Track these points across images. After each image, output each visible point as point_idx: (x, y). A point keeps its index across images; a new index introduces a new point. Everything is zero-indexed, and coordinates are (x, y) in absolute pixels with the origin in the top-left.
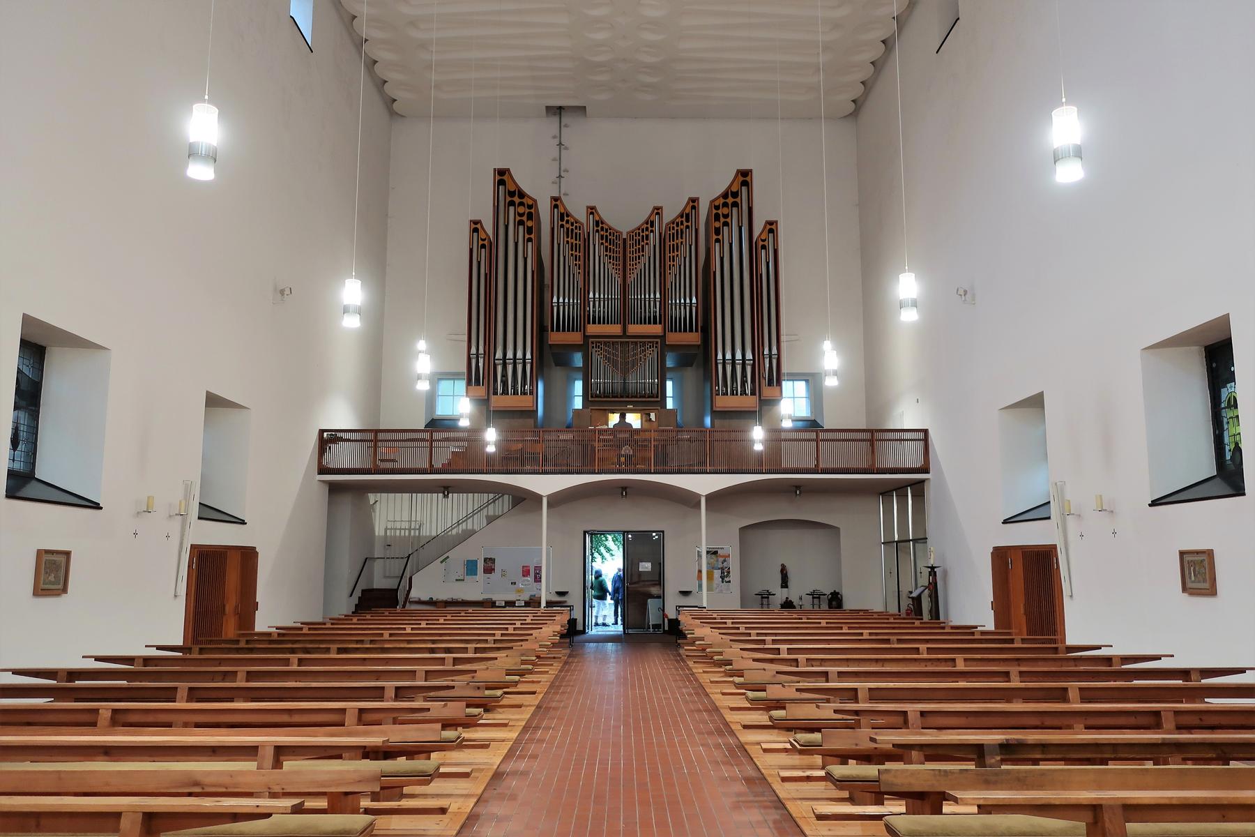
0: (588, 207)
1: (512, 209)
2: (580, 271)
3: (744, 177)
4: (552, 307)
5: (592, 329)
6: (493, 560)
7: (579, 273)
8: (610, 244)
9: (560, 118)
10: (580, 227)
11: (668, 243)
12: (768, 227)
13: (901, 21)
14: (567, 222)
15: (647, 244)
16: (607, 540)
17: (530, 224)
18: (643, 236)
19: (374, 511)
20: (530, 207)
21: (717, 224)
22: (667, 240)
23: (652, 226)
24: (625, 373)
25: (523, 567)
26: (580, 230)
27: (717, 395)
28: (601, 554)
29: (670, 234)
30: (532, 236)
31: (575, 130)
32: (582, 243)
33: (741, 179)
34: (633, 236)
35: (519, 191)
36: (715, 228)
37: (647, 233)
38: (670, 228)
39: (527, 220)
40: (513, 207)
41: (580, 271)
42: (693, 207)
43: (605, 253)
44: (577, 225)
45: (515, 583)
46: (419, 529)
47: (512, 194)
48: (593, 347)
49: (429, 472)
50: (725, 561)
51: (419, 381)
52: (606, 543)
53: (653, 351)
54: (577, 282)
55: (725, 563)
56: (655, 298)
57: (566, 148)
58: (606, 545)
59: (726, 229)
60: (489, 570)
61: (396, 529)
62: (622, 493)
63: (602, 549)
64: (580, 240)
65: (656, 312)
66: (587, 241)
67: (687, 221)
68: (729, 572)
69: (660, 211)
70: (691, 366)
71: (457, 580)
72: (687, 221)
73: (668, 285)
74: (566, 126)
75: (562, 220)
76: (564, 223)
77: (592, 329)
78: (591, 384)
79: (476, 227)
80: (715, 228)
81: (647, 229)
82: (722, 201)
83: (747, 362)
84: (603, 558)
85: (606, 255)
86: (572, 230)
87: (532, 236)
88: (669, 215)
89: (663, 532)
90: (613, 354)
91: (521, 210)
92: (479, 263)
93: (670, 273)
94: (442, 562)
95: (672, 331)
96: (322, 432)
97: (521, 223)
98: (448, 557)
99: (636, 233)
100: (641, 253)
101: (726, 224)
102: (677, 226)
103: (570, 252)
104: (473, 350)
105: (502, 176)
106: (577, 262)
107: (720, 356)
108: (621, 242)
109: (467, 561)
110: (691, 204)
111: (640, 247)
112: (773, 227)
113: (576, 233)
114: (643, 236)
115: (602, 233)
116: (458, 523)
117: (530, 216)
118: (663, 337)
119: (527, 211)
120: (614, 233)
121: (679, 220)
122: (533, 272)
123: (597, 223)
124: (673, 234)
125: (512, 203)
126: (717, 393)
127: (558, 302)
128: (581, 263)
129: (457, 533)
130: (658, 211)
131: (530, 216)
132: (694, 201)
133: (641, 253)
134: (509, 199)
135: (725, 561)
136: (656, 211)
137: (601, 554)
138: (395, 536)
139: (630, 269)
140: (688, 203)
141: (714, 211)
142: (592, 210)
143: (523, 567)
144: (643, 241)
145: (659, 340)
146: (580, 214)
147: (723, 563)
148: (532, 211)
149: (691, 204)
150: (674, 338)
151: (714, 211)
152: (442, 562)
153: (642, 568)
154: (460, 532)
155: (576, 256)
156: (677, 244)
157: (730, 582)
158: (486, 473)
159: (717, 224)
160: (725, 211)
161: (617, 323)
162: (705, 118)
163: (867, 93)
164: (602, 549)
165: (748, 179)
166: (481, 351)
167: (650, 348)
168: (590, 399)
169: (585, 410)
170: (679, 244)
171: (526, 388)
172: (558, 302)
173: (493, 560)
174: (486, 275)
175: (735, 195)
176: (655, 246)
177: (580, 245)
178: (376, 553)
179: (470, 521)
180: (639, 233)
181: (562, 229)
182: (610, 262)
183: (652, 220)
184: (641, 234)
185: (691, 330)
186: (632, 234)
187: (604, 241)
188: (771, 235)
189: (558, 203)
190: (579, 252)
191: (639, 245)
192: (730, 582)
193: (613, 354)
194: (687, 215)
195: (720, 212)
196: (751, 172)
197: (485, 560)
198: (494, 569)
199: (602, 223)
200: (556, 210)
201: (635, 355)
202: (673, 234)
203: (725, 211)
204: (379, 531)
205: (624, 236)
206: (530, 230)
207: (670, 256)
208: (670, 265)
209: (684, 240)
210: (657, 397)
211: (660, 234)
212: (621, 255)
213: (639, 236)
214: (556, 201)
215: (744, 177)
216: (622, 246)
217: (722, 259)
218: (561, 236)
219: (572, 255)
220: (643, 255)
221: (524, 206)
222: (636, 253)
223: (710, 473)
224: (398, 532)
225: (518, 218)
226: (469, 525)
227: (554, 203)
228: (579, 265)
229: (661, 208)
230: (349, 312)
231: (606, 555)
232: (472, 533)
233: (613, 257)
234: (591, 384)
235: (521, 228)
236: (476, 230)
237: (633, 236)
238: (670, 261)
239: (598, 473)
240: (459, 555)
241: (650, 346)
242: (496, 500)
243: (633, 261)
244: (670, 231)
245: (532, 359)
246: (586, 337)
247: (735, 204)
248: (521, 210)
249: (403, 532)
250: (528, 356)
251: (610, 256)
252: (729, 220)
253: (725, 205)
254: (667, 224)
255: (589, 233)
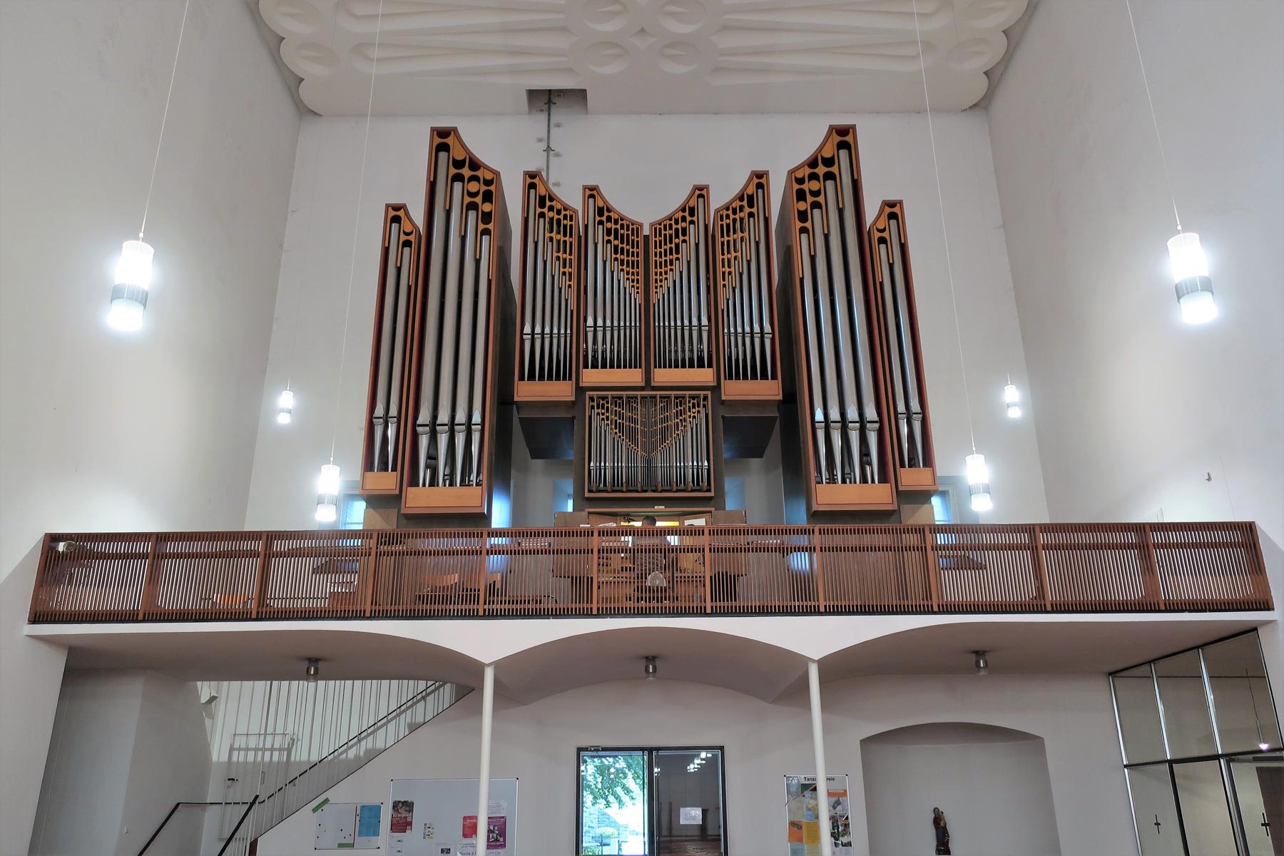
0: (585, 188)
1: (458, 186)
2: (572, 283)
3: (844, 137)
4: (522, 341)
5: (591, 377)
6: (409, 806)
7: (570, 286)
8: (622, 243)
9: (549, 114)
10: (571, 217)
11: (719, 240)
12: (888, 210)
13: (1013, 36)
14: (551, 208)
15: (684, 241)
16: (625, 778)
17: (487, 207)
18: (677, 230)
19: (212, 717)
20: (488, 183)
21: (802, 206)
22: (718, 235)
23: (692, 214)
24: (650, 449)
25: (465, 818)
26: (571, 220)
27: (818, 483)
28: (617, 798)
29: (722, 226)
30: (490, 226)
31: (566, 119)
32: (575, 240)
33: (837, 139)
34: (660, 229)
35: (471, 159)
36: (799, 211)
37: (684, 225)
38: (722, 216)
39: (483, 203)
40: (461, 184)
41: (572, 283)
42: (760, 186)
43: (614, 256)
44: (568, 213)
45: (448, 851)
46: (289, 750)
47: (458, 164)
48: (593, 407)
49: (254, 616)
50: (838, 803)
51: (116, 302)
52: (624, 781)
53: (699, 412)
54: (567, 300)
55: (839, 808)
56: (700, 325)
57: (558, 155)
58: (624, 785)
59: (816, 212)
60: (401, 825)
61: (247, 749)
62: (647, 669)
63: (619, 790)
64: (571, 236)
65: (702, 351)
66: (583, 242)
67: (751, 205)
68: (846, 826)
69: (704, 192)
70: (759, 454)
71: (341, 846)
72: (751, 205)
73: (722, 304)
74: (558, 126)
75: (542, 205)
76: (545, 210)
77: (591, 377)
78: (590, 471)
79: (396, 214)
80: (799, 211)
81: (684, 219)
82: (808, 171)
83: (868, 425)
84: (620, 802)
85: (616, 259)
86: (559, 220)
87: (490, 226)
88: (718, 200)
89: (722, 748)
90: (630, 419)
91: (473, 187)
92: (399, 270)
93: (724, 286)
94: (315, 810)
95: (731, 378)
96: (53, 538)
97: (473, 206)
98: (326, 801)
99: (665, 226)
100: (675, 256)
101: (815, 205)
102: (734, 212)
103: (548, 235)
104: (379, 411)
105: (443, 139)
106: (566, 270)
107: (819, 416)
108: (641, 240)
109: (363, 807)
110: (756, 181)
111: (673, 246)
112: (896, 210)
113: (565, 226)
114: (677, 230)
115: (609, 225)
116: (360, 737)
117: (488, 197)
118: (716, 389)
119: (484, 188)
120: (628, 226)
121: (737, 204)
122: (489, 281)
123: (600, 212)
124: (728, 225)
125: (458, 178)
126: (819, 480)
127: (533, 333)
128: (574, 270)
129: (356, 756)
130: (701, 192)
131: (488, 197)
132: (760, 179)
133: (675, 256)
134: (453, 171)
135: (838, 803)
136: (698, 192)
137: (617, 798)
138: (246, 763)
139: (656, 280)
140: (750, 180)
141: (796, 187)
142: (592, 192)
143: (465, 818)
144: (677, 237)
145: (709, 393)
146: (571, 197)
147: (834, 807)
148: (492, 188)
149: (756, 181)
150: (735, 390)
151: (796, 187)
152: (315, 810)
153: (686, 819)
154: (362, 754)
155: (565, 260)
156: (735, 241)
157: (849, 844)
158: (370, 618)
159: (802, 206)
160: (814, 185)
161: (635, 367)
162: (762, 113)
163: (1007, 59)
164: (619, 790)
165: (849, 138)
166: (393, 411)
167: (694, 407)
168: (587, 495)
169: (578, 513)
170: (739, 241)
171: (471, 479)
172: (533, 333)
173: (409, 806)
174: (409, 287)
175: (829, 162)
176: (697, 245)
177: (571, 243)
178: (208, 798)
179: (381, 732)
180: (671, 225)
181: (542, 220)
182: (622, 270)
183: (692, 205)
184: (674, 227)
185: (764, 376)
186: (658, 226)
187: (612, 238)
188: (893, 222)
189: (536, 181)
190: (570, 254)
191: (671, 243)
192: (849, 844)
193: (630, 419)
194: (750, 198)
195: (805, 187)
196: (853, 128)
197: (396, 805)
198: (410, 824)
199: (609, 211)
200: (532, 191)
201: (666, 419)
202: (728, 225)
203: (814, 185)
204: (219, 753)
205: (646, 231)
206: (487, 217)
207: (723, 260)
208: (724, 273)
209: (746, 234)
210: (709, 490)
211: (706, 227)
212: (641, 258)
213: (671, 229)
214: (532, 180)
215: (844, 137)
216: (641, 245)
217: (813, 259)
218: (540, 229)
219: (558, 258)
220: (677, 259)
221: (479, 182)
222: (666, 256)
223: (828, 612)
224: (268, 754)
225: (468, 200)
226: (380, 740)
227: (529, 181)
228: (570, 274)
229: (707, 187)
230: (323, 503)
231: (625, 798)
232: (372, 755)
233: (628, 261)
234: (590, 471)
235: (472, 214)
236: (396, 219)
237: (660, 229)
238: (723, 266)
239: (598, 616)
240: (347, 795)
241: (694, 404)
242: (428, 695)
243: (661, 268)
244: (722, 220)
245: (483, 424)
246: (580, 390)
247: (830, 176)
248: (473, 187)
249: (276, 754)
250: (477, 418)
251: (622, 261)
252: (821, 199)
253: (813, 177)
254: (717, 211)
255: (586, 227)
